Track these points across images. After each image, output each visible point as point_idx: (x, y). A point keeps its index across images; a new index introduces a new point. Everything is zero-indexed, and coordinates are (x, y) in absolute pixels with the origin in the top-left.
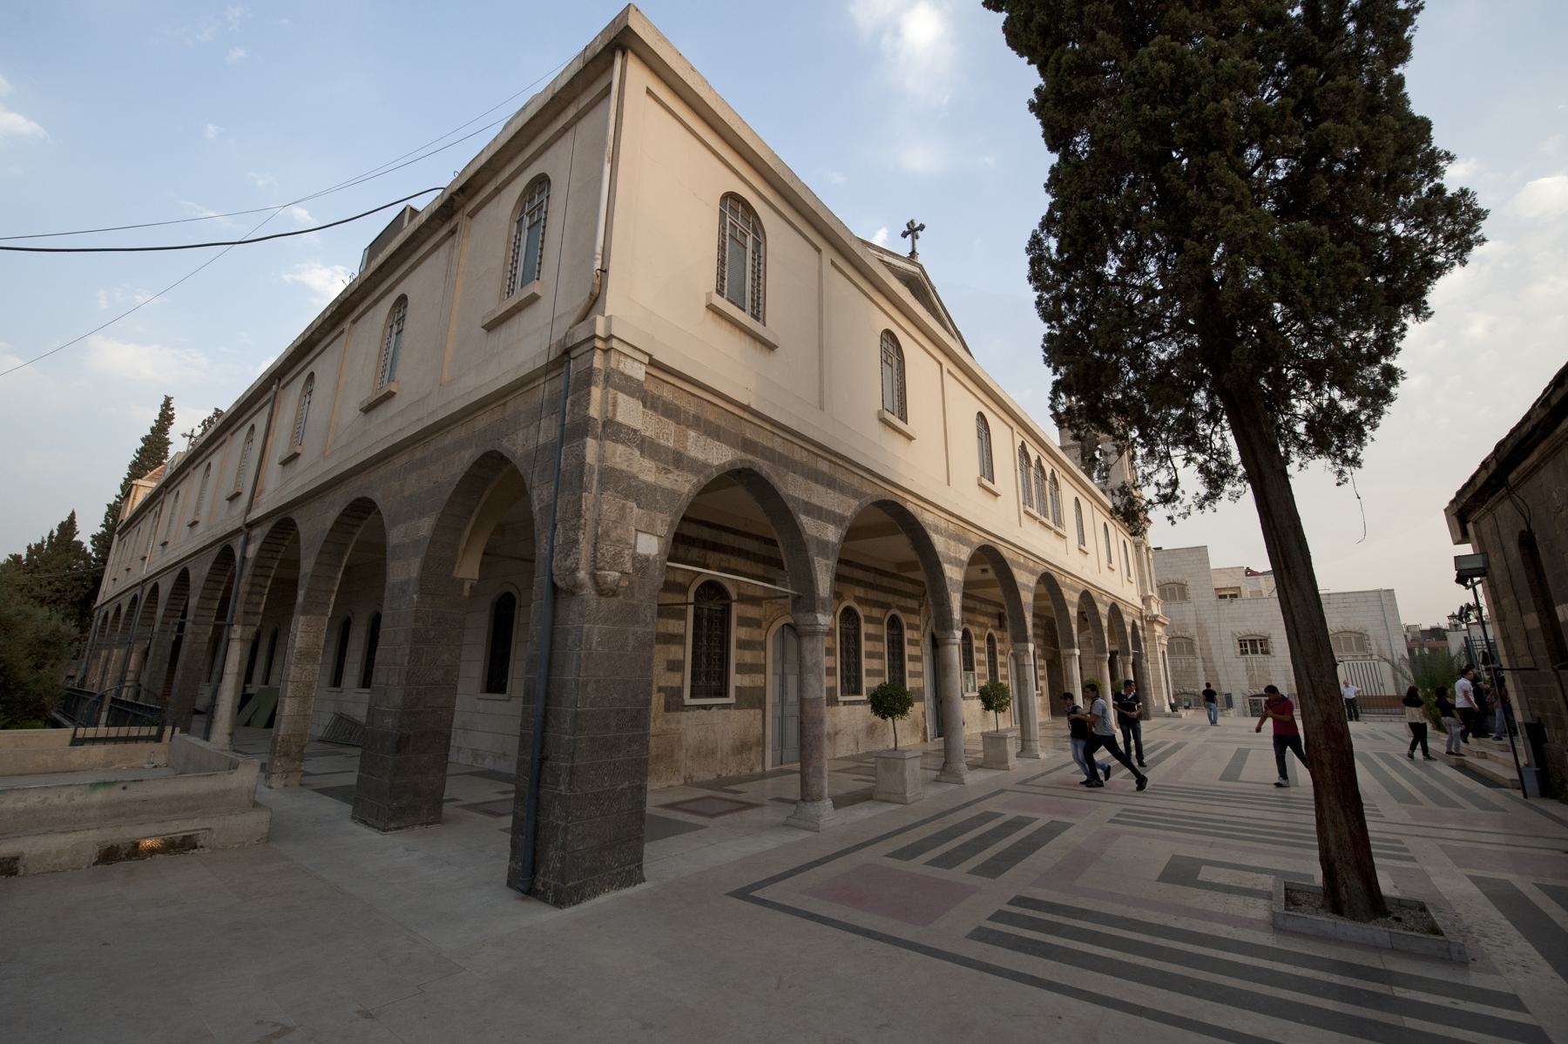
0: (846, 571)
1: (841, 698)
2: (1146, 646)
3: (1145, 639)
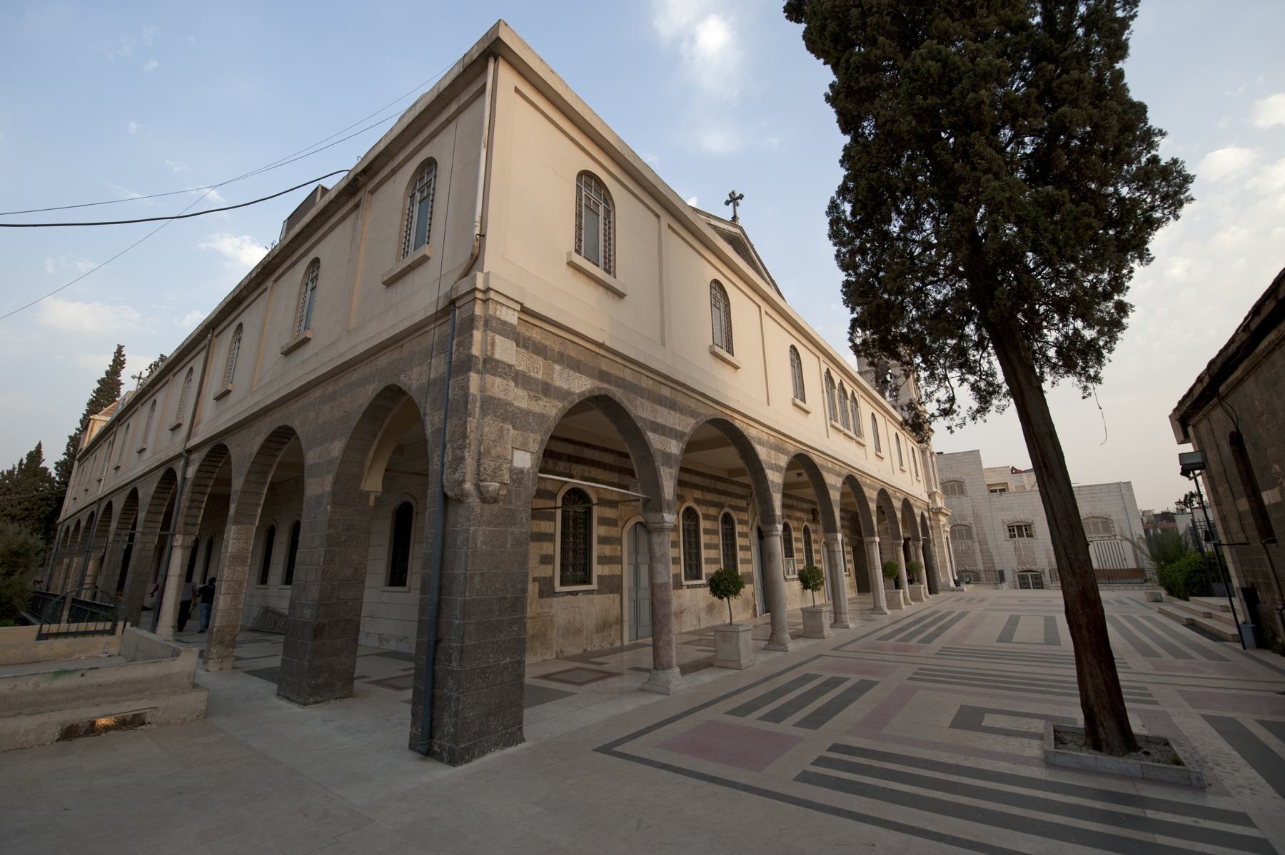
0: (687, 477)
1: (685, 583)
2: (933, 533)
3: (932, 527)
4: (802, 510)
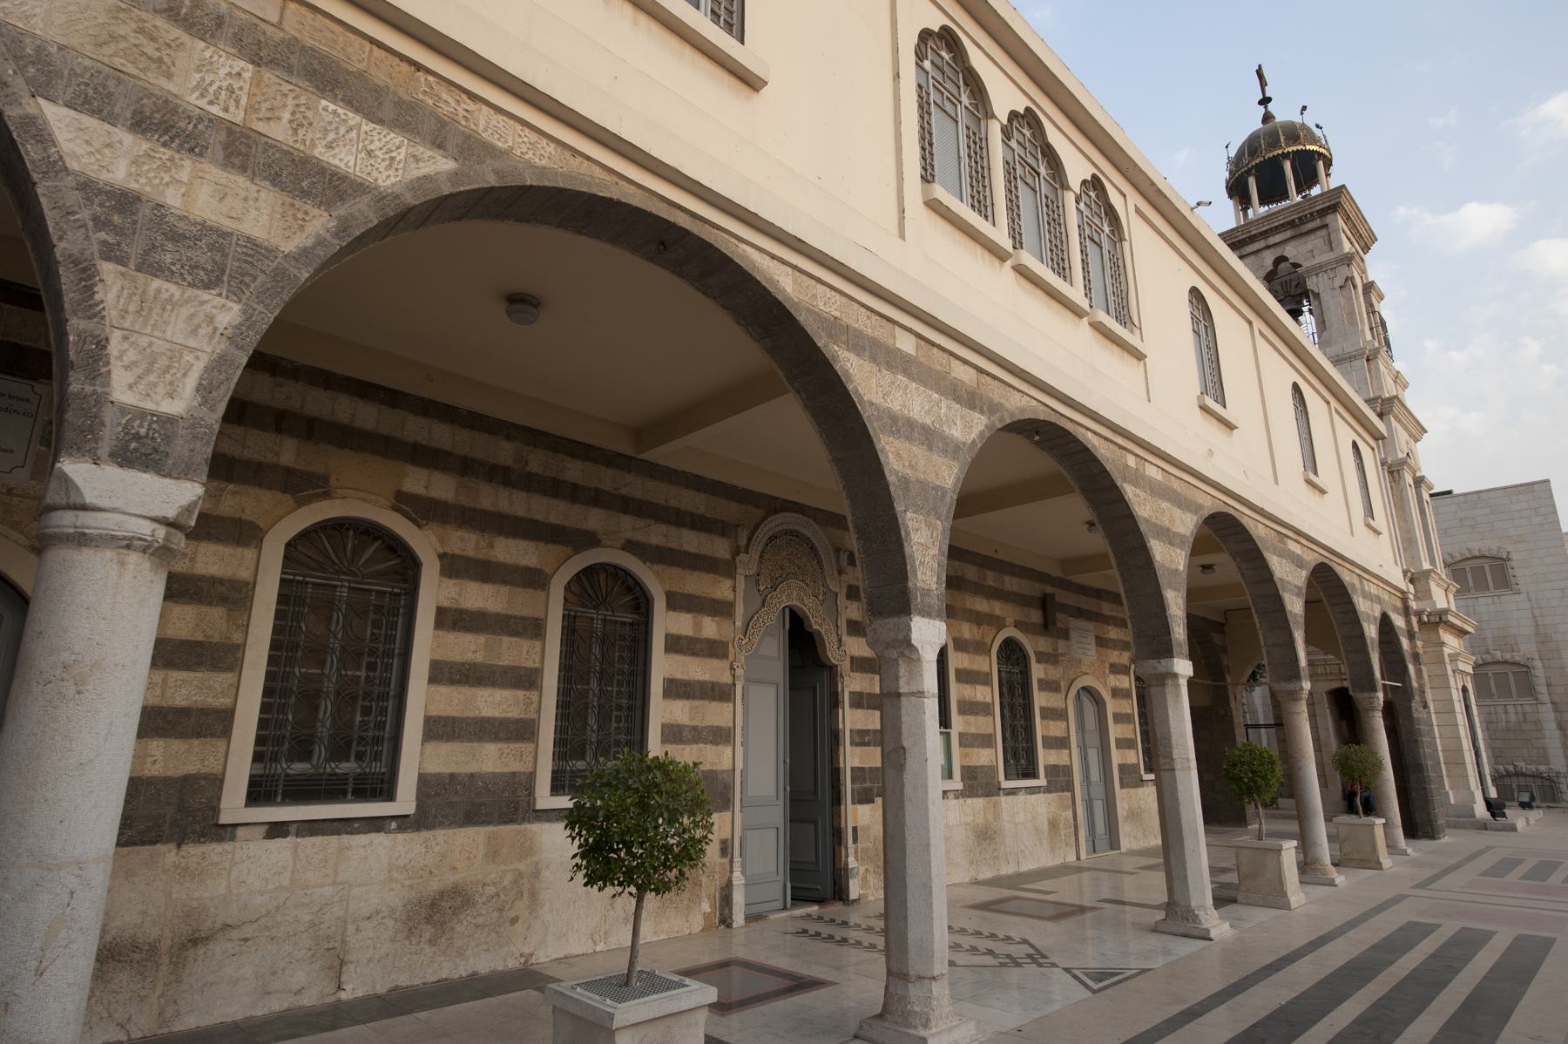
1: (1006, 784)
2: (1419, 672)
3: (1416, 657)
4: (994, 594)
